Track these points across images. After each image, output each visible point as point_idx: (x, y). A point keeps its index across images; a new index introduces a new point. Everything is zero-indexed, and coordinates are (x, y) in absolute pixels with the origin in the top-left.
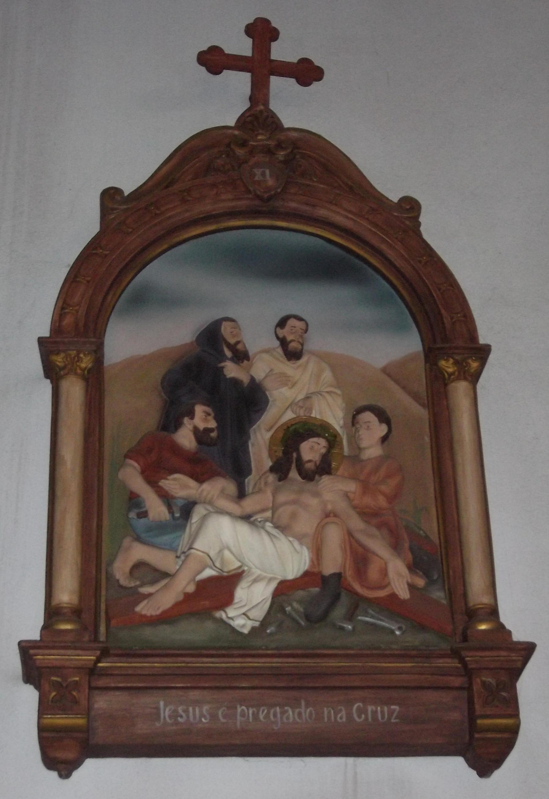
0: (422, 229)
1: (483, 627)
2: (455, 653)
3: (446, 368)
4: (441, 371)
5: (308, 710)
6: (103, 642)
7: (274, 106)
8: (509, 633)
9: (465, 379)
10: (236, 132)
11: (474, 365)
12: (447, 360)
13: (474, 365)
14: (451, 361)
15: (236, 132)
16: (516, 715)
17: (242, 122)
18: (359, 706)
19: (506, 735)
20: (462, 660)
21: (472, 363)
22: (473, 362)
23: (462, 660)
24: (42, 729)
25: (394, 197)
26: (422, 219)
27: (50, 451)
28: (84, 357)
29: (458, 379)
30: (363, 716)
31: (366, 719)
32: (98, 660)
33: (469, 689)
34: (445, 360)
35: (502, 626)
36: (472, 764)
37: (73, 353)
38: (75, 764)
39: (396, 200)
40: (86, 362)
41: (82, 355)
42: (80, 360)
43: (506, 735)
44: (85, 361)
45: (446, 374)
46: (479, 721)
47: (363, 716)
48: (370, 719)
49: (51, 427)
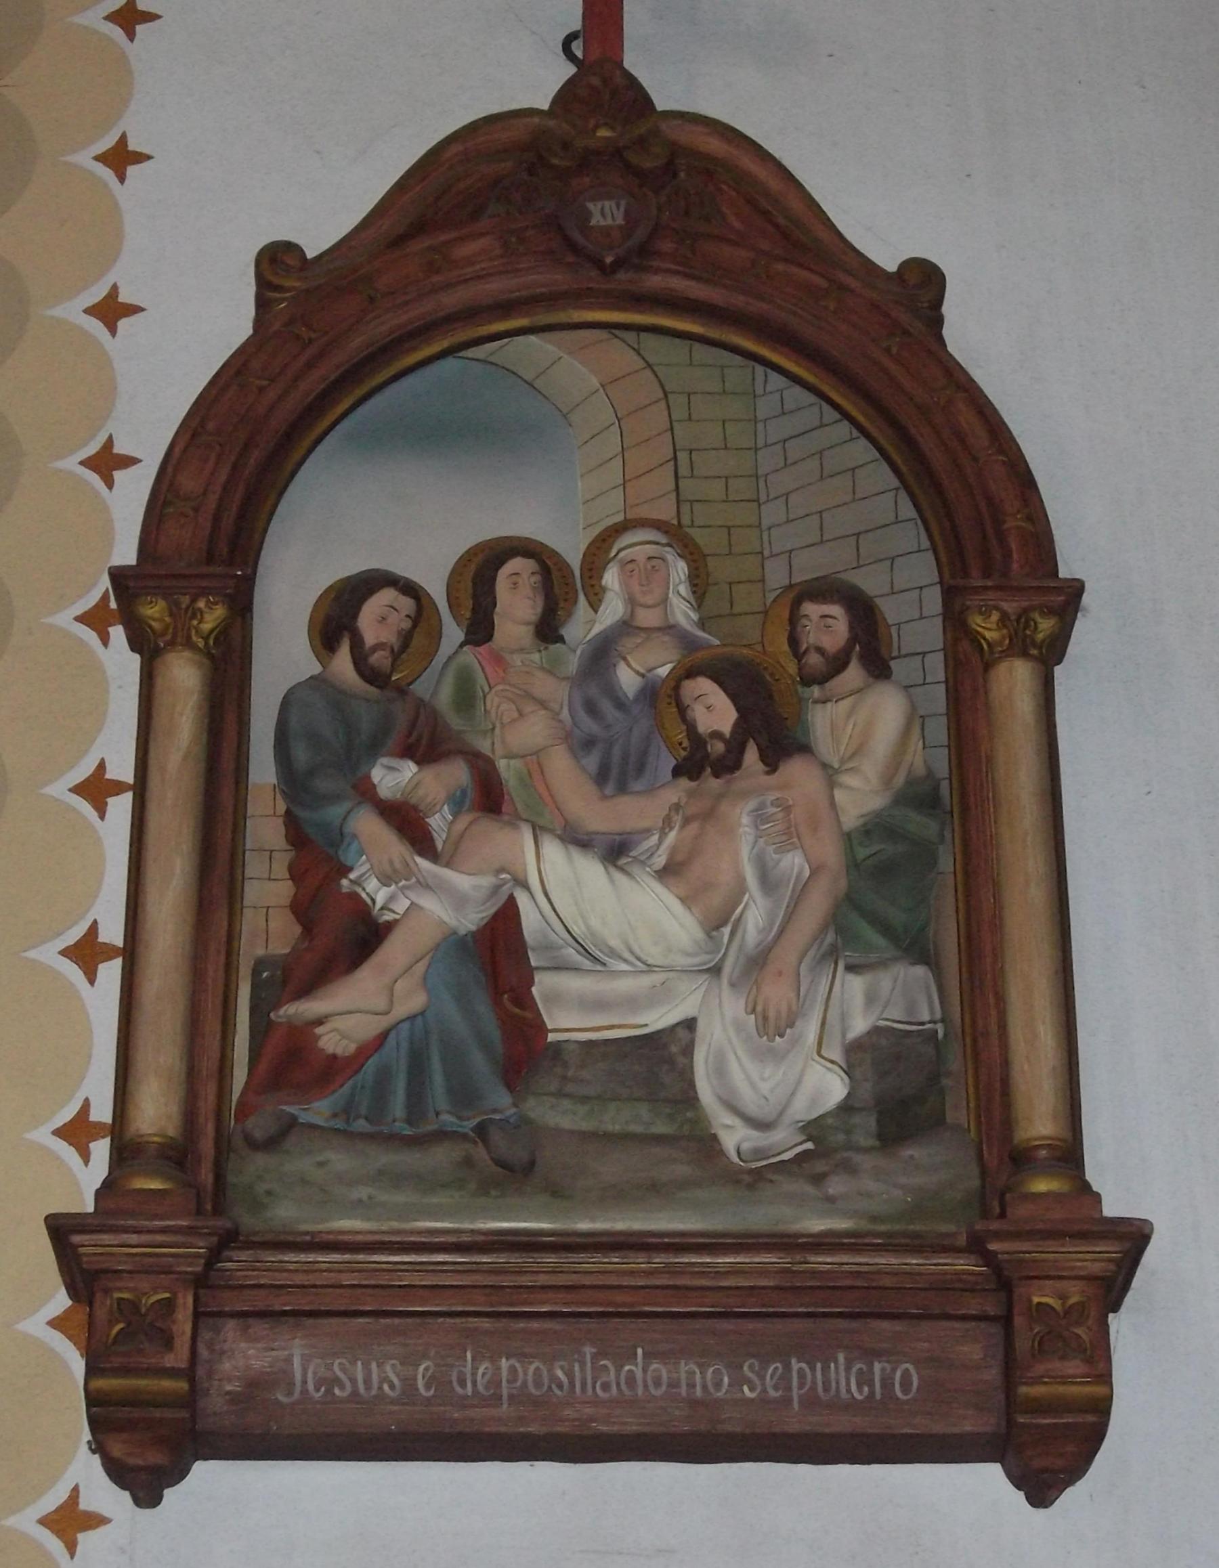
0: (946, 332)
1: (1041, 1186)
2: (976, 1246)
3: (988, 635)
4: (975, 639)
5: (532, 1368)
6: (997, 608)
7: (633, 62)
8: (1097, 1198)
9: (1025, 654)
10: (552, 123)
11: (1045, 626)
12: (986, 615)
13: (1045, 626)
14: (995, 616)
15: (552, 123)
16: (1105, 1378)
17: (566, 96)
18: (861, 1369)
19: (1091, 1418)
20: (988, 1258)
21: (1039, 620)
22: (1042, 617)
23: (988, 1258)
24: (93, 1399)
25: (889, 263)
26: (949, 309)
27: (123, 970)
28: (206, 610)
29: (1008, 653)
30: (866, 1389)
31: (872, 1393)
32: (215, 1255)
33: (1006, 1320)
34: (981, 613)
35: (1086, 1187)
36: (1018, 1481)
37: (185, 600)
38: (178, 1474)
39: (891, 266)
40: (212, 616)
41: (201, 604)
42: (196, 614)
43: (1091, 1418)
44: (207, 617)
45: (985, 646)
46: (1023, 1390)
47: (866, 1389)
48: (878, 1396)
49: (117, 1058)
